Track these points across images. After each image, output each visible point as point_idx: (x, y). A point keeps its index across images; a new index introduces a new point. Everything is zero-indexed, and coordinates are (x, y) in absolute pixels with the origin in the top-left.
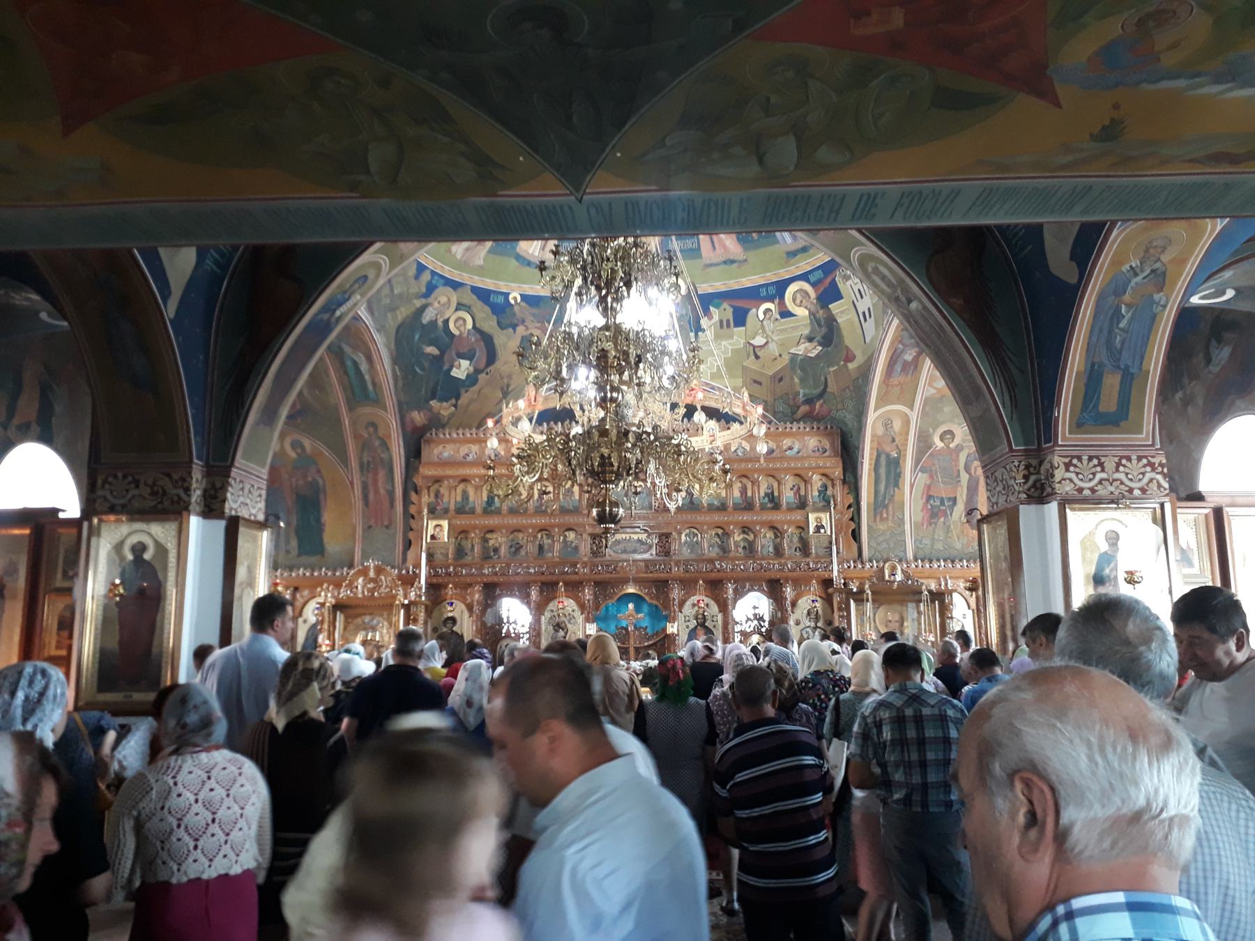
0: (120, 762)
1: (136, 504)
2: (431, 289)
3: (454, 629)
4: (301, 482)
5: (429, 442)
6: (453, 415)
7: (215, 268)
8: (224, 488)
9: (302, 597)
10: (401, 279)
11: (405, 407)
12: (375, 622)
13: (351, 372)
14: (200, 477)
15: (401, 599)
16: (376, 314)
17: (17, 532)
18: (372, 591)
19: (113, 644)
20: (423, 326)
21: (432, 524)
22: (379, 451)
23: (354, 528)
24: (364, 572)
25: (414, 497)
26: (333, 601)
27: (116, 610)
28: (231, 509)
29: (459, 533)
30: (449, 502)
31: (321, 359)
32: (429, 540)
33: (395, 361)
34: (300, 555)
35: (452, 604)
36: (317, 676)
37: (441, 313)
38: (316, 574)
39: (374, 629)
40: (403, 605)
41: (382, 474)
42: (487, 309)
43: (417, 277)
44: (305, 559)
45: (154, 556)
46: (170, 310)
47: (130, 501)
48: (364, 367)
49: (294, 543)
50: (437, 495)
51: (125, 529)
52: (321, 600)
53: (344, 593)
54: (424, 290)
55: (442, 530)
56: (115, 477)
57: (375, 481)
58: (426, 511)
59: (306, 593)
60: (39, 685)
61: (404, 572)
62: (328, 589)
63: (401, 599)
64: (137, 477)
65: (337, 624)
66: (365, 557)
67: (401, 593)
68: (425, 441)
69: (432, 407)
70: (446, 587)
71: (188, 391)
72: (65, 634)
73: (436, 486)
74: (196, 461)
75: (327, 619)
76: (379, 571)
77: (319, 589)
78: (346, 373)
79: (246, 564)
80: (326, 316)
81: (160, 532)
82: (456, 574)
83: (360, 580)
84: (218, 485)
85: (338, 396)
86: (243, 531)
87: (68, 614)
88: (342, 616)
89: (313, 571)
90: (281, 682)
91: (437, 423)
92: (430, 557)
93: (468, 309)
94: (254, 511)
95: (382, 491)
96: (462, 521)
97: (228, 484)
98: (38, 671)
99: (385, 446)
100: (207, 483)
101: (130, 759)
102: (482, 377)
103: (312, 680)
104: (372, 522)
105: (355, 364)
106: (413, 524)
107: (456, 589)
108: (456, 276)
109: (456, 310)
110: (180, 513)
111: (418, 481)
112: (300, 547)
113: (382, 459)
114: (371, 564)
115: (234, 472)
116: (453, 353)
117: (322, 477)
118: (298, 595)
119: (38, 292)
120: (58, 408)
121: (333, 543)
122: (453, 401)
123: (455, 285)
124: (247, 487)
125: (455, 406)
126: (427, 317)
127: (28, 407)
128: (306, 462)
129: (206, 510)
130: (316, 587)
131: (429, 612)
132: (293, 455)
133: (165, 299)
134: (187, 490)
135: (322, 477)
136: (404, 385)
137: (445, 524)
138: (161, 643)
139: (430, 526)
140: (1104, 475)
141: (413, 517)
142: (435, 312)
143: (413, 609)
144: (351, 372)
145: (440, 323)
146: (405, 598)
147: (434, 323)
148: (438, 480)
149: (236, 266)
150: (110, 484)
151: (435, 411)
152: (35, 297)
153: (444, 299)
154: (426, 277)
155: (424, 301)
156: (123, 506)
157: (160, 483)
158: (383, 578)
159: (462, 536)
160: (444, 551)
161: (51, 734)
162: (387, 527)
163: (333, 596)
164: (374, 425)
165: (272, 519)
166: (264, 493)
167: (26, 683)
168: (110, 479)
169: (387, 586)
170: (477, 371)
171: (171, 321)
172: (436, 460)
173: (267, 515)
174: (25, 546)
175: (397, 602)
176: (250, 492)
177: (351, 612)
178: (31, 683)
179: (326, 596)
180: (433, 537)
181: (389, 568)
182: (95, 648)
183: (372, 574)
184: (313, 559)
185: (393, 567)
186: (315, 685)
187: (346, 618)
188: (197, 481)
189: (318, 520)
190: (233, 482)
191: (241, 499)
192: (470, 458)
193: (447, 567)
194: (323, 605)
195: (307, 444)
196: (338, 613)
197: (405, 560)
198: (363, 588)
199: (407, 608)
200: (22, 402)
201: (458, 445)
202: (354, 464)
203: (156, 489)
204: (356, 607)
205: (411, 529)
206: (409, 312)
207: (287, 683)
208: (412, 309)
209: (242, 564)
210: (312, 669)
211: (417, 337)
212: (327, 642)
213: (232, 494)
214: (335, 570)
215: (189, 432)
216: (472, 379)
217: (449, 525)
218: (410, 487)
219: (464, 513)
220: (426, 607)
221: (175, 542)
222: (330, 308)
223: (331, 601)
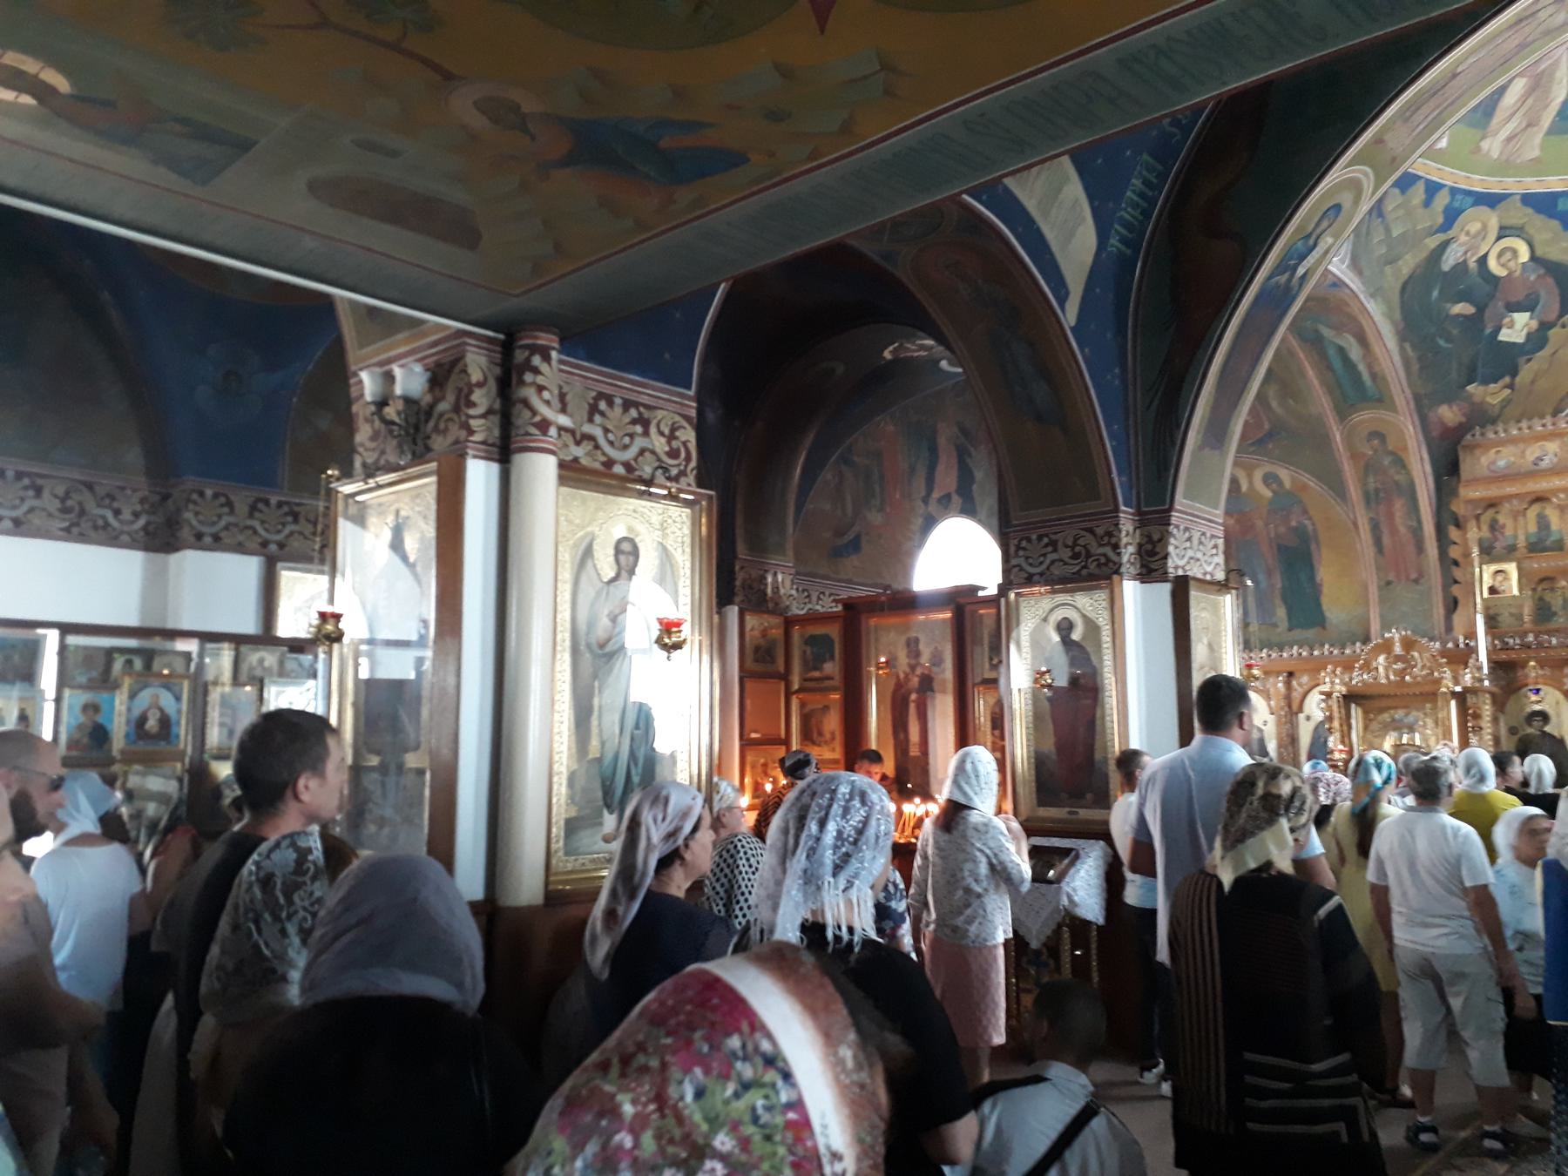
0: (1069, 897)
1: (1057, 571)
2: (1451, 216)
3: (1547, 729)
4: (1282, 529)
5: (1471, 448)
6: (1506, 403)
7: (1123, 248)
8: (1163, 539)
9: (1300, 685)
10: (1401, 212)
11: (1426, 401)
12: (1410, 719)
13: (1337, 364)
14: (1131, 529)
15: (1448, 684)
16: (1367, 273)
17: (941, 616)
18: (1401, 673)
19: (1049, 745)
20: (1446, 274)
21: (1489, 570)
22: (1392, 471)
23: (1366, 588)
24: (1386, 647)
25: (1454, 533)
26: (1344, 690)
27: (1046, 704)
28: (1176, 568)
29: (1537, 584)
30: (1516, 537)
31: (1283, 340)
32: (1486, 595)
33: (1402, 338)
34: (1290, 630)
35: (1538, 691)
36: (1287, 809)
37: (1472, 248)
38: (1316, 653)
39: (1411, 730)
40: (1454, 694)
41: (1399, 506)
42: (1555, 224)
43: (1427, 203)
44: (1298, 634)
45: (1084, 637)
46: (1070, 315)
47: (1048, 568)
48: (1355, 353)
49: (1281, 612)
50: (1494, 526)
51: (1046, 603)
52: (1326, 688)
53: (1358, 678)
54: (1440, 220)
55: (1507, 579)
56: (1029, 540)
57: (1391, 516)
58: (1475, 552)
59: (1305, 679)
60: (856, 818)
61: (1450, 645)
62: (1334, 672)
63: (1448, 684)
64: (1054, 537)
65: (1353, 722)
66: (1386, 626)
67: (1448, 674)
68: (1464, 447)
69: (1470, 396)
70: (1524, 665)
71: (1103, 412)
72: (997, 732)
73: (1490, 512)
74: (1123, 508)
75: (1336, 715)
76: (1408, 645)
77: (1323, 674)
78: (1330, 367)
79: (1205, 641)
80: (1283, 279)
81: (1088, 604)
82: (1540, 645)
83: (1381, 659)
84: (1156, 537)
85: (1321, 402)
86: (1195, 596)
87: (997, 710)
88: (1360, 711)
89: (1312, 649)
90: (1228, 809)
91: (1481, 418)
92: (1492, 622)
93: (1518, 231)
94: (1209, 569)
95: (1402, 530)
96: (1541, 564)
97: (1170, 534)
98: (857, 792)
99: (1401, 463)
100: (1141, 535)
101: (1081, 893)
102: (1553, 333)
103: (1278, 815)
104: (1391, 577)
105: (1342, 351)
106: (1457, 573)
107: (1542, 667)
108: (1493, 185)
109: (1499, 238)
110: (1109, 578)
111: (1458, 507)
112: (1290, 619)
113: (1397, 483)
114: (1395, 635)
115: (1175, 518)
116: (1501, 304)
117: (1310, 519)
118: (1294, 683)
119: (936, 339)
120: (979, 475)
121: (1336, 607)
122: (1507, 379)
123: (1491, 201)
124: (1196, 536)
125: (1511, 386)
126: (1449, 261)
127: (947, 477)
128: (1285, 502)
129: (1144, 571)
130: (1318, 671)
131: (1499, 704)
132: (1268, 493)
133: (1062, 302)
134: (1116, 547)
135: (1310, 519)
136: (1422, 368)
137: (1512, 568)
138: (1105, 748)
139: (1486, 575)
140: (231, 519)
141: (1456, 563)
142: (1463, 249)
143: (1471, 700)
144: (1337, 364)
145: (1472, 264)
146: (1457, 683)
147: (1462, 267)
148: (1492, 504)
149: (1150, 244)
150: (1024, 549)
151: (1477, 399)
152: (929, 342)
153: (1475, 227)
154: (1442, 200)
155: (1441, 237)
156: (1041, 574)
157: (1081, 542)
158: (1416, 654)
159: (1545, 585)
160: (1513, 610)
161: (870, 891)
162: (1416, 581)
163: (1343, 683)
164: (1382, 437)
165: (1233, 576)
166: (1221, 542)
167: (840, 811)
168: (1024, 544)
169: (1424, 667)
170: (1545, 326)
171: (1072, 329)
172: (1486, 473)
173: (1228, 572)
174: (948, 632)
175: (1444, 690)
176: (1201, 543)
177: (1377, 704)
178: (846, 811)
179: (1332, 683)
180: (1492, 590)
181: (1424, 641)
182: (1028, 752)
183: (1398, 649)
184: (1310, 633)
185: (1432, 639)
186: (1284, 823)
187: (1366, 712)
188: (1127, 535)
189: (1312, 578)
190: (1175, 531)
191: (1190, 553)
192: (1545, 464)
193: (1524, 634)
194: (1328, 695)
195: (1285, 475)
196: (1353, 706)
197: (1449, 628)
198: (1386, 669)
199: (1461, 698)
200: (940, 469)
201: (1521, 446)
202: (1354, 492)
203: (1077, 549)
204: (1381, 696)
205: (1456, 582)
206: (1417, 260)
207: (1239, 812)
208: (1424, 255)
209: (1200, 640)
210: (1279, 797)
211: (1435, 294)
212: (1341, 747)
213: (1176, 547)
214: (1343, 647)
215: (1110, 473)
216: (1537, 340)
217: (1520, 569)
218: (1446, 520)
219: (1545, 550)
220: (1493, 695)
221: (1106, 614)
222: (1287, 265)
223: (1340, 689)
